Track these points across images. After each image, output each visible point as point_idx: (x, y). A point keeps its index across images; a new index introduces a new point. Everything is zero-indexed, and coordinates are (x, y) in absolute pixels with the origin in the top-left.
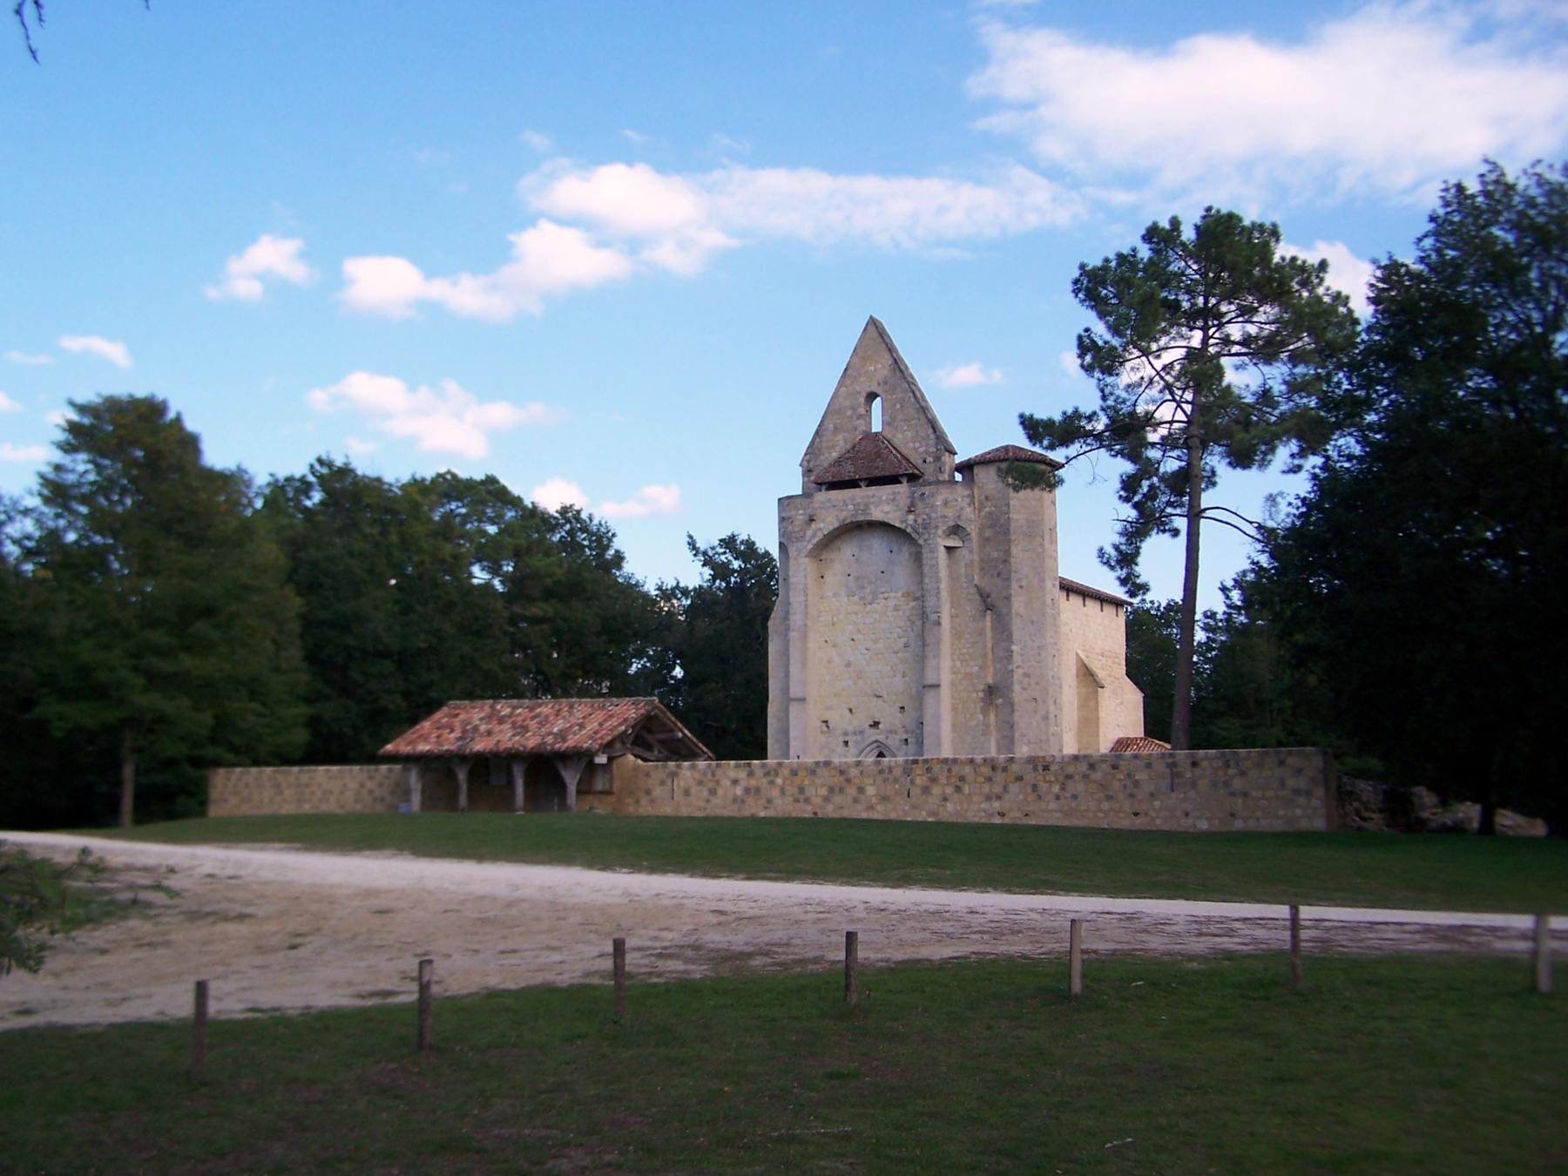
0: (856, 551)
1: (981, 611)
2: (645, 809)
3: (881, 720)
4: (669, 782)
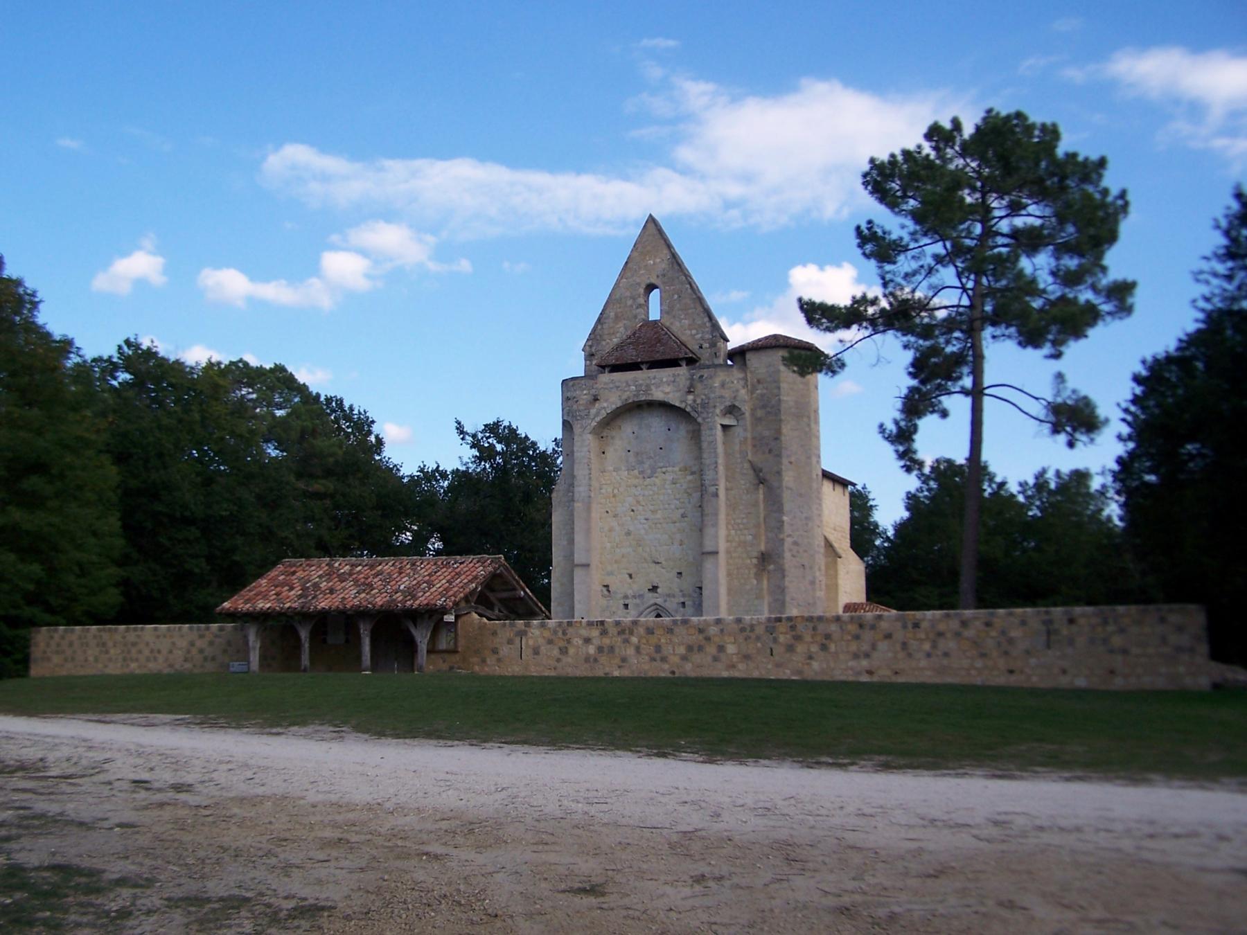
0: (636, 429)
2: (492, 668)
3: (660, 585)
4: (517, 640)
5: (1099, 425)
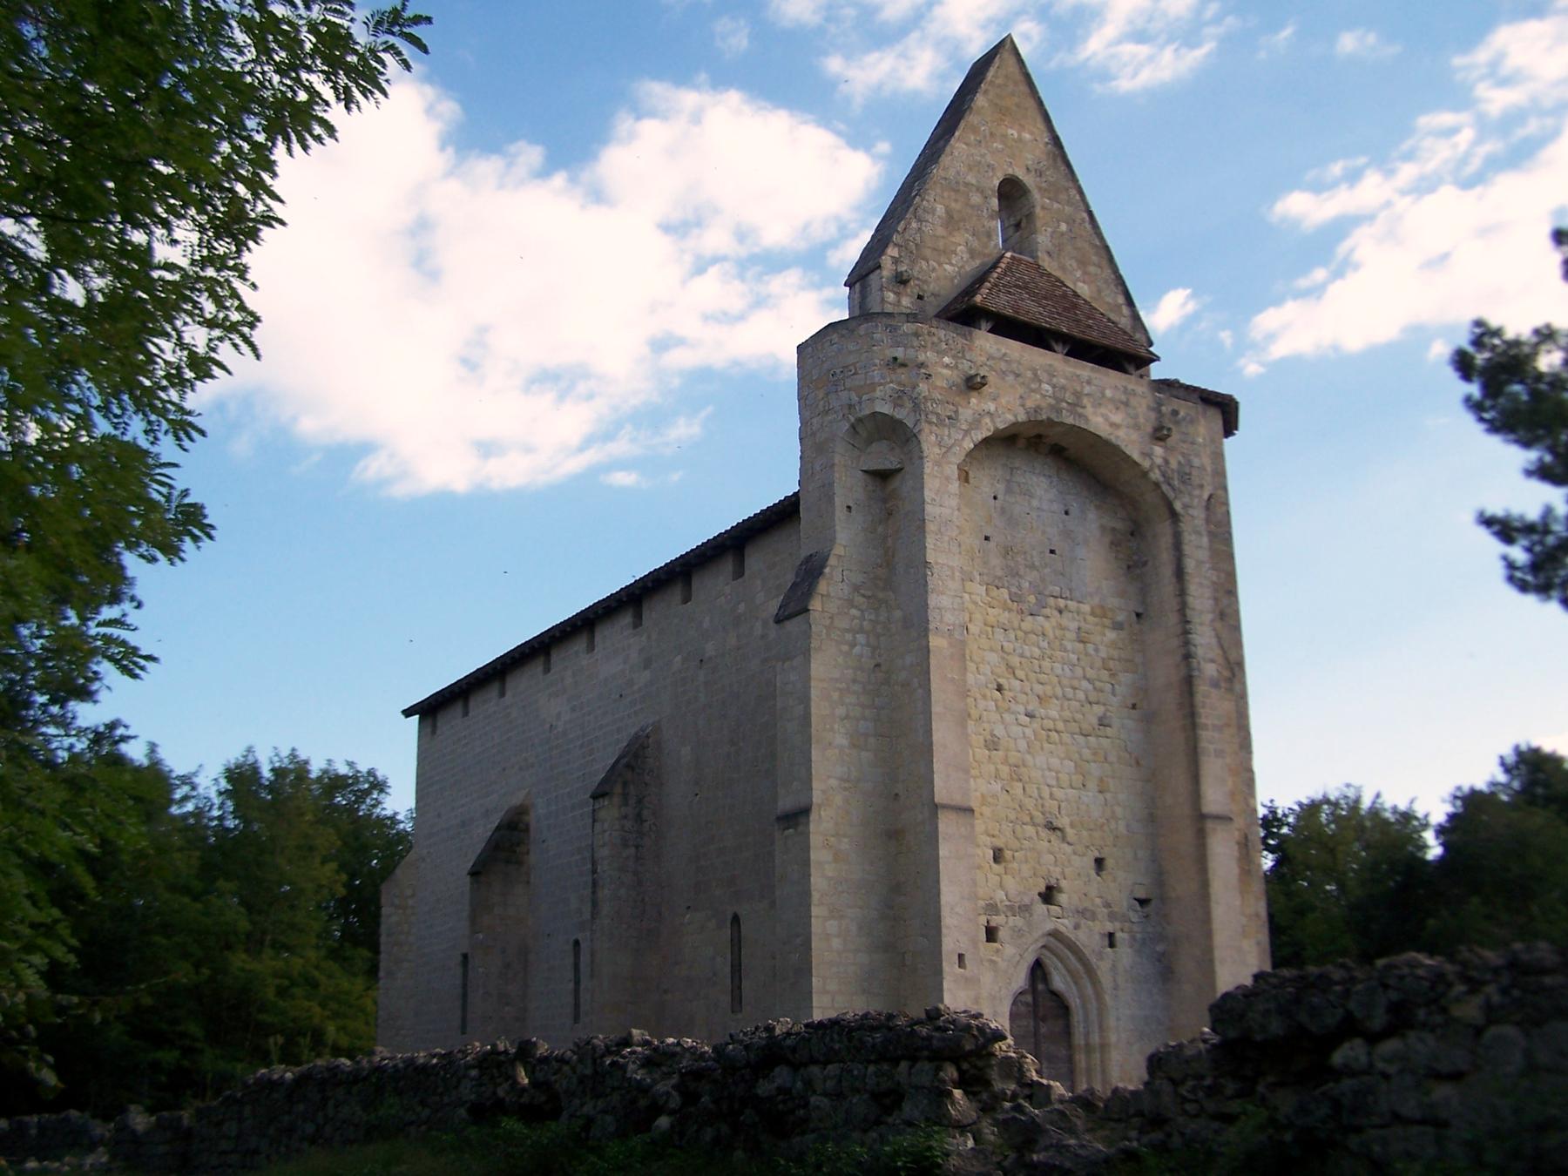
0: (1000, 488)
3: (1064, 884)
5: (251, 760)
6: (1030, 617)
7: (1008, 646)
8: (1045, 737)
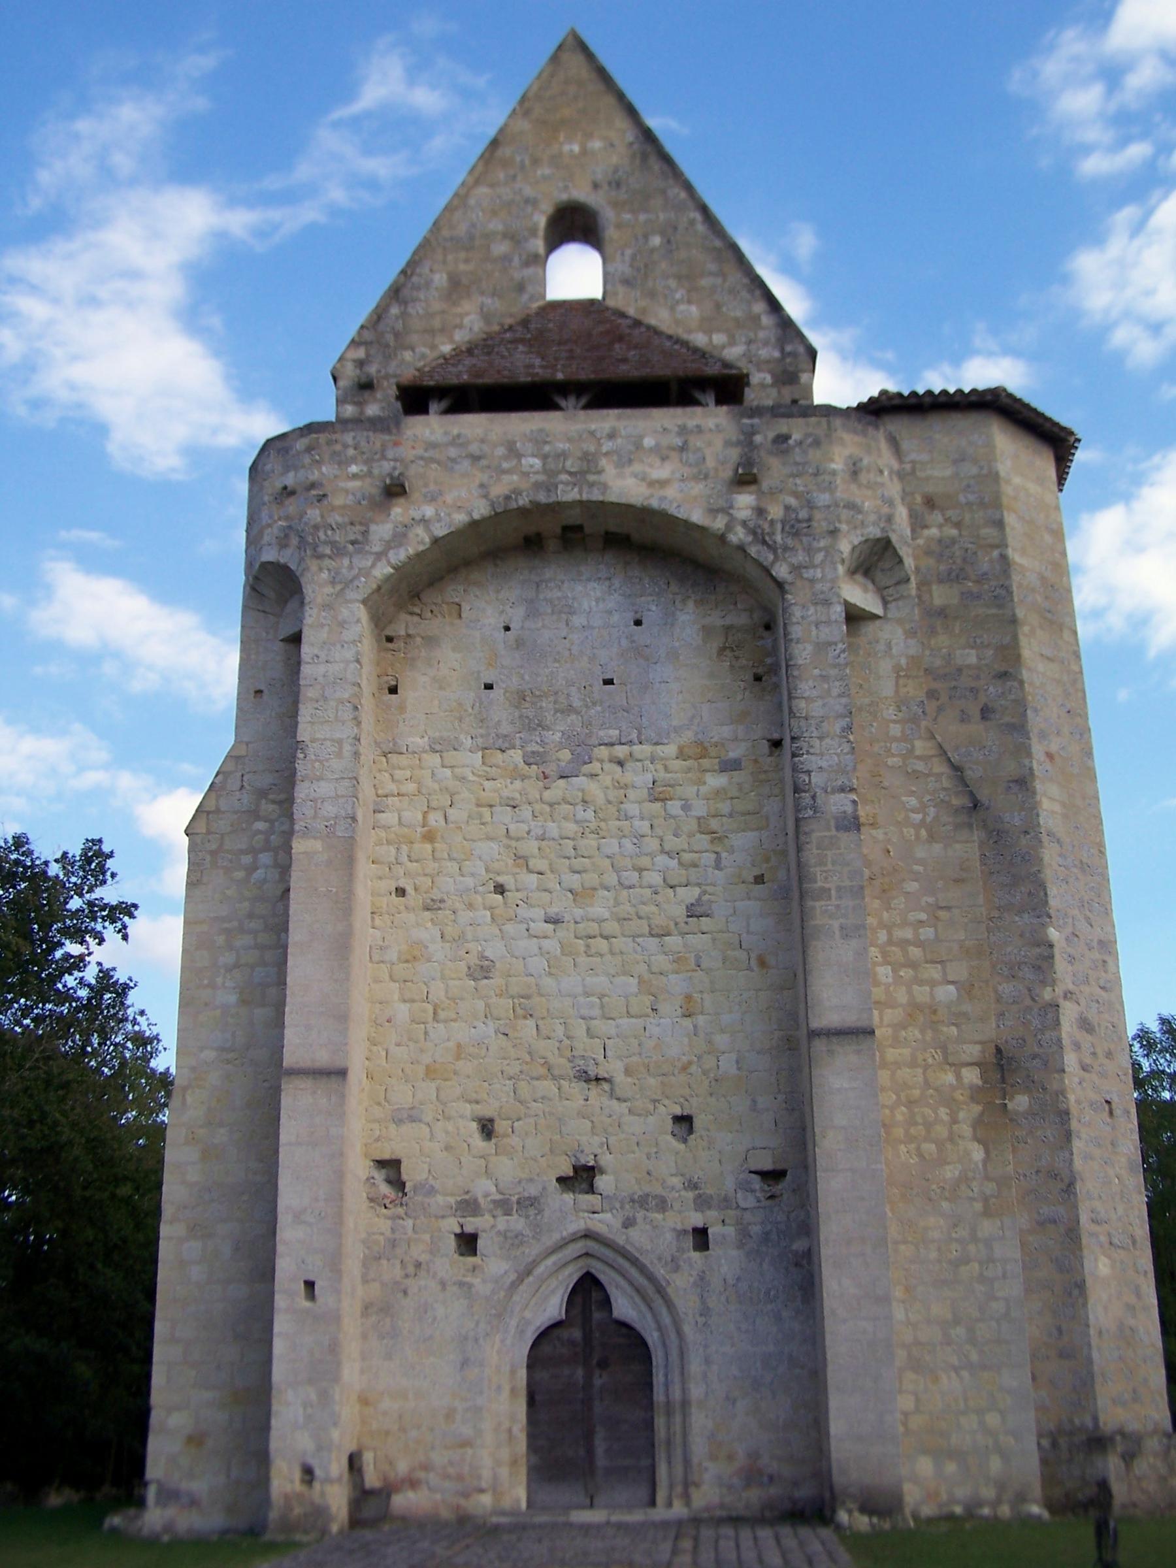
0: (516, 616)
1: (957, 811)
3: (606, 1160)
6: (562, 781)
7: (515, 828)
8: (583, 949)
